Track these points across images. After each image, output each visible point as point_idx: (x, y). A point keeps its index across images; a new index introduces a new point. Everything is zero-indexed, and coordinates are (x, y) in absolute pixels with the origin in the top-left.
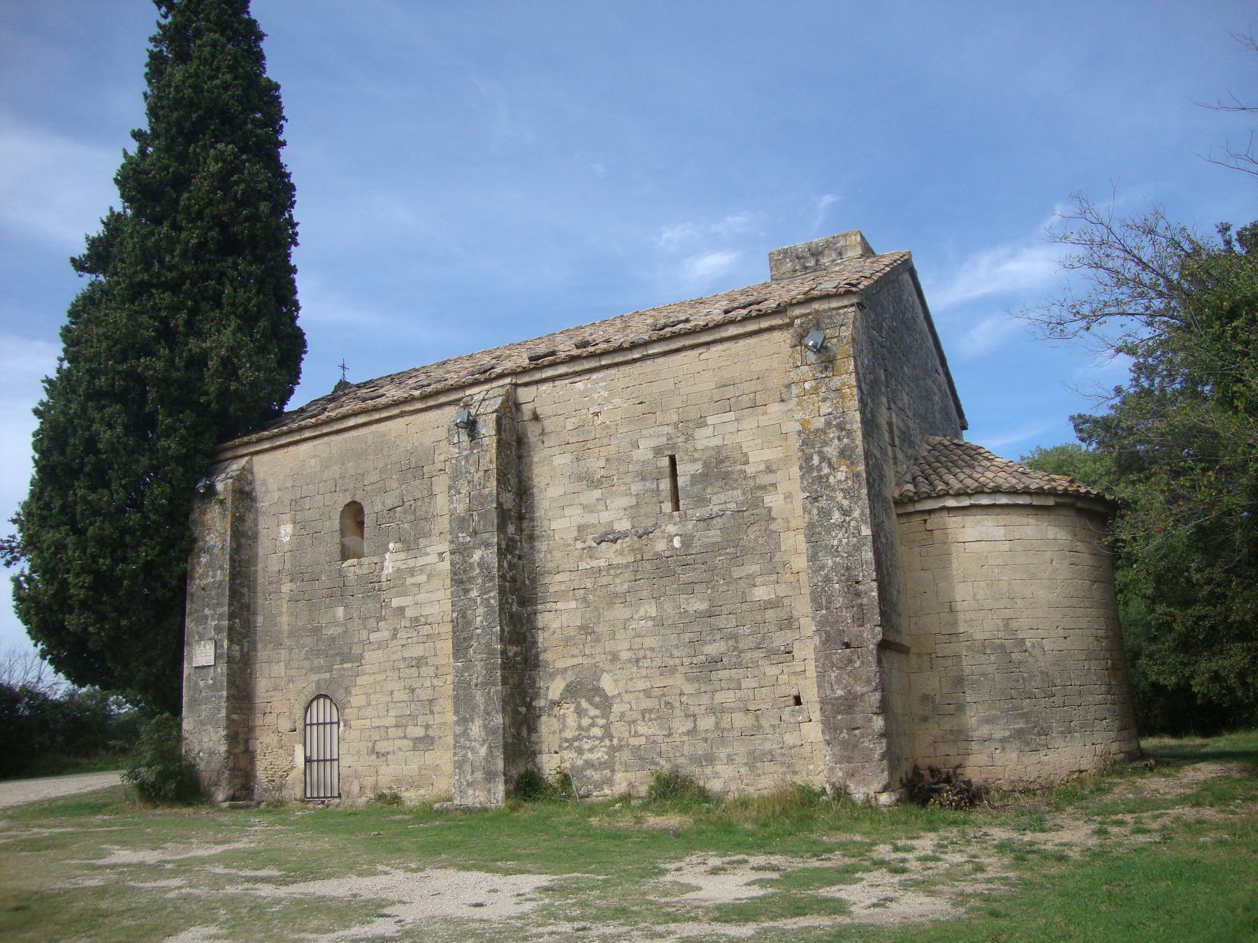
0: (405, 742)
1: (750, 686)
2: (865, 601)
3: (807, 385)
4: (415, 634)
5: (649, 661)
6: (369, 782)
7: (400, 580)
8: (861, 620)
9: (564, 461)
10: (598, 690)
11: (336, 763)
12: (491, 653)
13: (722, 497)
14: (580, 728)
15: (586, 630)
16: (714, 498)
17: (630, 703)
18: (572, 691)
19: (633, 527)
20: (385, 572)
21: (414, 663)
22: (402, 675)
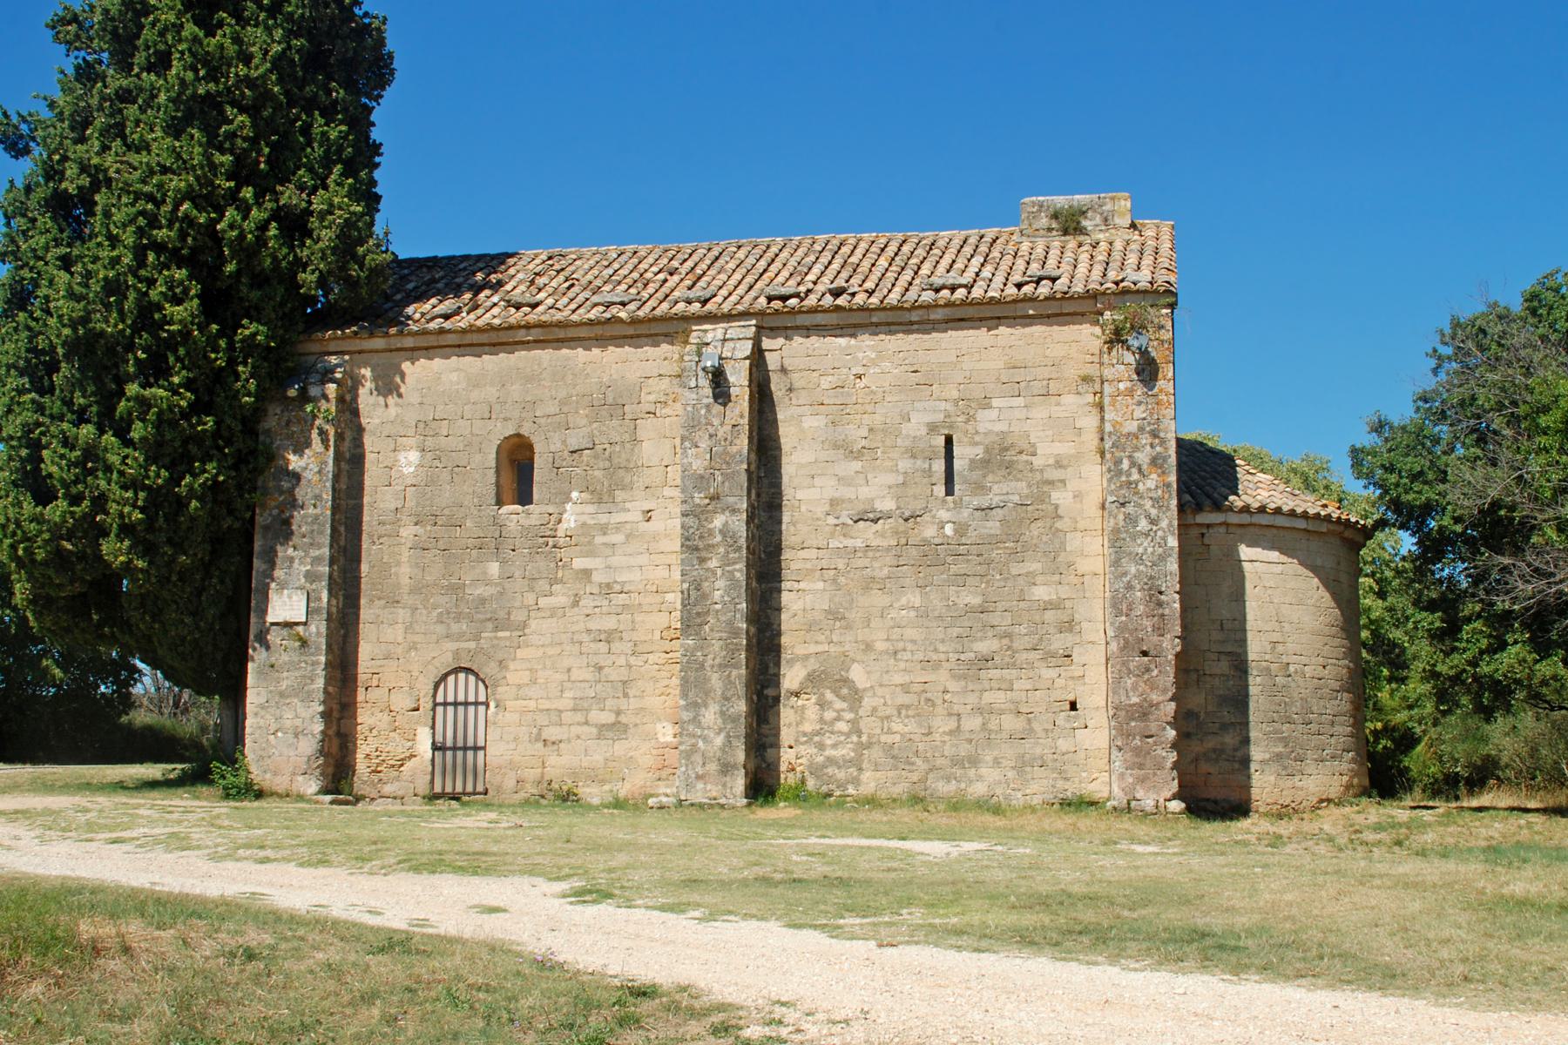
0: (585, 728)
1: (1024, 687)
2: (1167, 611)
3: (1122, 386)
4: (606, 603)
5: (909, 654)
6: (531, 774)
7: (584, 539)
8: (1160, 631)
9: (816, 424)
10: (846, 681)
12: (735, 633)
15: (834, 615)
16: (995, 487)
17: (884, 697)
18: (814, 680)
19: (898, 508)
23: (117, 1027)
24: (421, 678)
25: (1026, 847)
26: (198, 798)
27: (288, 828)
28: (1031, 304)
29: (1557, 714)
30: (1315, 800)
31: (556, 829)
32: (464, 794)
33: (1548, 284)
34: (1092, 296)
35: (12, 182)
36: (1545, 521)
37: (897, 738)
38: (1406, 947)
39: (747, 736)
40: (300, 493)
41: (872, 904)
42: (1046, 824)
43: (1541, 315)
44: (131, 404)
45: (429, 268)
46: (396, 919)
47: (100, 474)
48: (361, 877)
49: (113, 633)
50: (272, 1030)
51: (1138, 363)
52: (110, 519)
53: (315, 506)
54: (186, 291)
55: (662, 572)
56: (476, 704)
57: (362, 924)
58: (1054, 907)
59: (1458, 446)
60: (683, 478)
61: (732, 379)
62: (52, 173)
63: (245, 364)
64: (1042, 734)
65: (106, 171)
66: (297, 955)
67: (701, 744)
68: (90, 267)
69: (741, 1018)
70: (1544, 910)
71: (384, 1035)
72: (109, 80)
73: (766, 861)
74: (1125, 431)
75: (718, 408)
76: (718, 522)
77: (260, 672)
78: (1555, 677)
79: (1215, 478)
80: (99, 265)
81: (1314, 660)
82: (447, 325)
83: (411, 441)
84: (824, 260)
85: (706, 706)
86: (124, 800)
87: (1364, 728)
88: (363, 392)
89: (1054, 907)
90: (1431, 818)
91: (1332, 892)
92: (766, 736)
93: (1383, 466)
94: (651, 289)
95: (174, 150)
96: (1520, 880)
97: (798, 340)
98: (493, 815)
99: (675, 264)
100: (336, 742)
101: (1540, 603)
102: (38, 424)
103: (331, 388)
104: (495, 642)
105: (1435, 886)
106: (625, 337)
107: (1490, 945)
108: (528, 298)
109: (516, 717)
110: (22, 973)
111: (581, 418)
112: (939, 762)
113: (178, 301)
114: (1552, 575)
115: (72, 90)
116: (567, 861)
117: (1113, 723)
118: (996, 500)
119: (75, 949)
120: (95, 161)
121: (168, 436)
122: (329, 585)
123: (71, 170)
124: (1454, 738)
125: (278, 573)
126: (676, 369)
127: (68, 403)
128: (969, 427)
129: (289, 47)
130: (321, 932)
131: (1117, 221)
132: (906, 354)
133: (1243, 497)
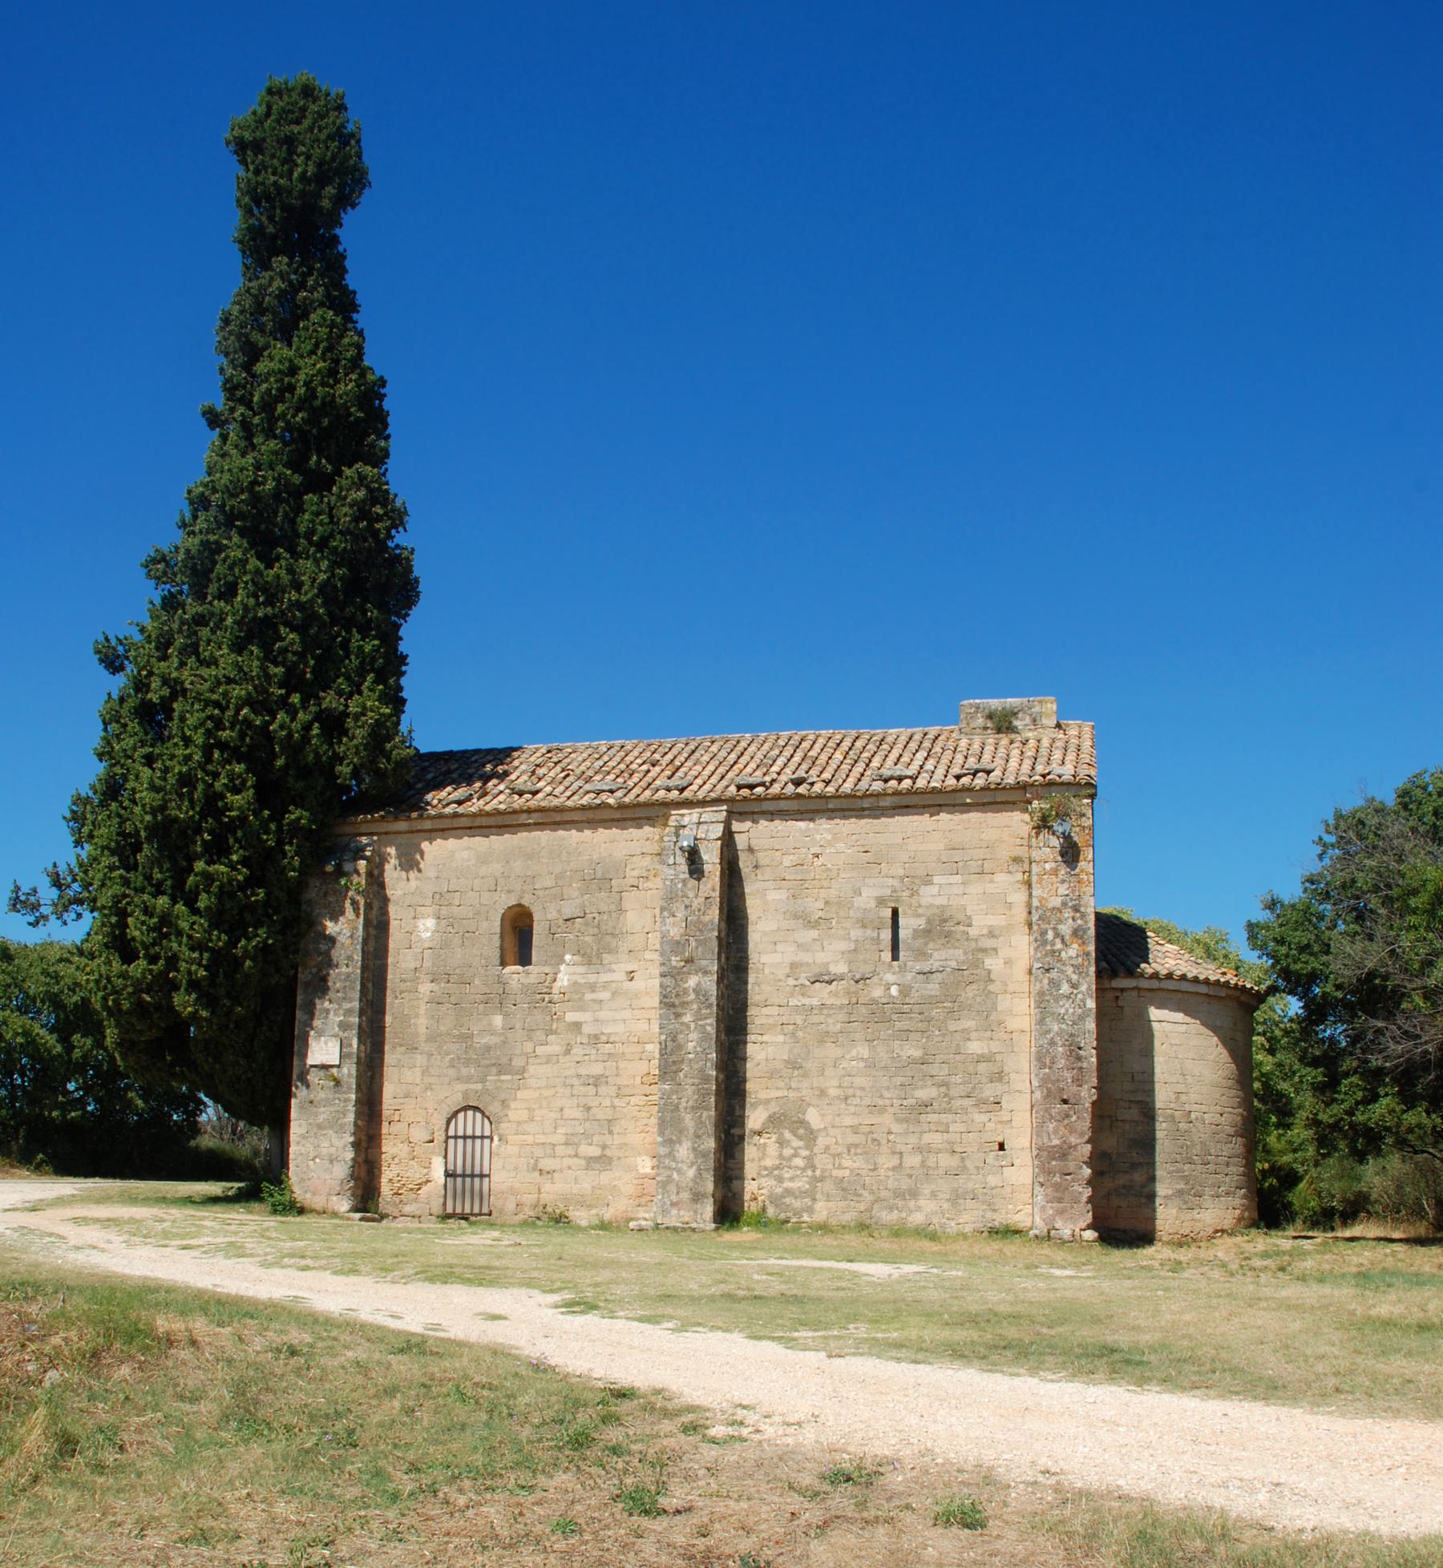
0: (576, 1160)
2: (1085, 1065)
3: (1048, 866)
4: (594, 1051)
6: (529, 1199)
7: (576, 995)
8: (1078, 1081)
10: (803, 1123)
11: (487, 1179)
12: (706, 1079)
13: (943, 954)
14: (781, 1156)
15: (793, 1064)
18: (774, 1121)
19: (850, 971)
20: (558, 984)
21: (591, 1081)
22: (575, 1092)
23: (187, 1407)
24: (436, 1114)
25: (958, 1270)
26: (251, 1212)
27: (324, 1241)
28: (968, 794)
29: (1420, 1157)
30: (1211, 1231)
31: (550, 1248)
32: (472, 1214)
33: (1417, 784)
34: (1022, 787)
35: (109, 694)
36: (1413, 990)
37: (847, 1173)
38: (1287, 1363)
39: (716, 1170)
40: (335, 954)
41: (822, 1319)
42: (976, 1249)
43: (1411, 810)
44: (198, 878)
45: (446, 761)
46: (413, 1324)
47: (173, 938)
48: (385, 1285)
49: (183, 1072)
50: (312, 1417)
51: (1062, 847)
52: (179, 976)
53: (347, 965)
54: (244, 782)
55: (643, 1026)
56: (482, 1137)
57: (385, 1327)
58: (983, 1324)
59: (1340, 922)
60: (662, 943)
61: (705, 857)
62: (141, 686)
63: (291, 844)
64: (973, 1171)
65: (182, 683)
66: (331, 1352)
67: (675, 1175)
68: (168, 763)
69: (707, 1419)
70: (1405, 1329)
71: (404, 1424)
72: (187, 607)
73: (732, 1279)
74: (1050, 906)
75: (693, 883)
76: (692, 982)
77: (301, 1107)
78: (1419, 1126)
79: (1128, 948)
80: (175, 762)
81: (1213, 1108)
82: (460, 810)
83: (430, 910)
84: (787, 753)
85: (680, 1143)
86: (193, 1213)
87: (1254, 1166)
88: (388, 868)
89: (983, 1324)
90: (1311, 1247)
91: (1224, 1313)
92: (732, 1170)
93: (1275, 939)
94: (635, 779)
95: (237, 665)
96: (1385, 1302)
97: (763, 823)
98: (496, 1234)
99: (657, 756)
100: (364, 1168)
101: (1408, 1060)
102: (125, 896)
103: (362, 863)
104: (499, 1084)
105: (1313, 1307)
106: (613, 820)
107: (1359, 1360)
108: (529, 786)
109: (516, 1149)
110: (113, 1357)
111: (574, 890)
112: (884, 1194)
113: (237, 791)
114: (1418, 1037)
115: (158, 617)
116: (559, 1275)
117: (1036, 1162)
118: (936, 966)
119: (153, 1340)
120: (174, 675)
121: (228, 906)
122: (359, 1033)
123: (155, 683)
124: (1332, 1176)
125: (317, 1023)
126: (656, 848)
127: (148, 878)
128: (913, 901)
129: (333, 575)
130: (351, 1333)
131: (1045, 721)
132: (858, 837)
133: (1153, 965)
